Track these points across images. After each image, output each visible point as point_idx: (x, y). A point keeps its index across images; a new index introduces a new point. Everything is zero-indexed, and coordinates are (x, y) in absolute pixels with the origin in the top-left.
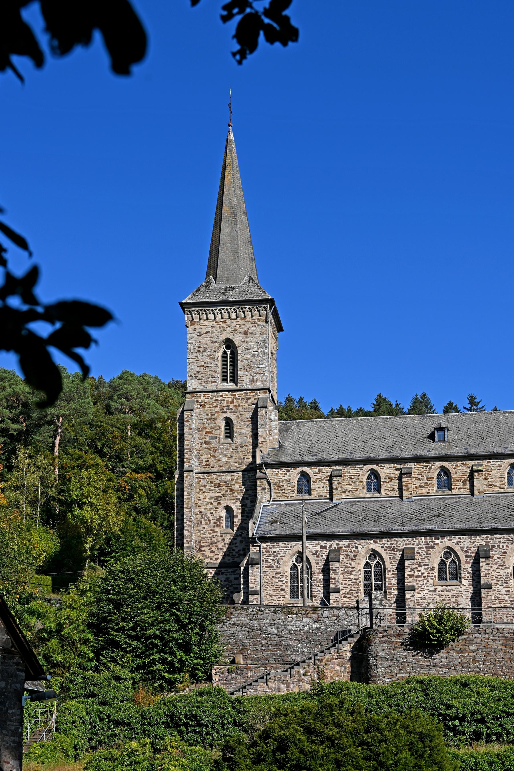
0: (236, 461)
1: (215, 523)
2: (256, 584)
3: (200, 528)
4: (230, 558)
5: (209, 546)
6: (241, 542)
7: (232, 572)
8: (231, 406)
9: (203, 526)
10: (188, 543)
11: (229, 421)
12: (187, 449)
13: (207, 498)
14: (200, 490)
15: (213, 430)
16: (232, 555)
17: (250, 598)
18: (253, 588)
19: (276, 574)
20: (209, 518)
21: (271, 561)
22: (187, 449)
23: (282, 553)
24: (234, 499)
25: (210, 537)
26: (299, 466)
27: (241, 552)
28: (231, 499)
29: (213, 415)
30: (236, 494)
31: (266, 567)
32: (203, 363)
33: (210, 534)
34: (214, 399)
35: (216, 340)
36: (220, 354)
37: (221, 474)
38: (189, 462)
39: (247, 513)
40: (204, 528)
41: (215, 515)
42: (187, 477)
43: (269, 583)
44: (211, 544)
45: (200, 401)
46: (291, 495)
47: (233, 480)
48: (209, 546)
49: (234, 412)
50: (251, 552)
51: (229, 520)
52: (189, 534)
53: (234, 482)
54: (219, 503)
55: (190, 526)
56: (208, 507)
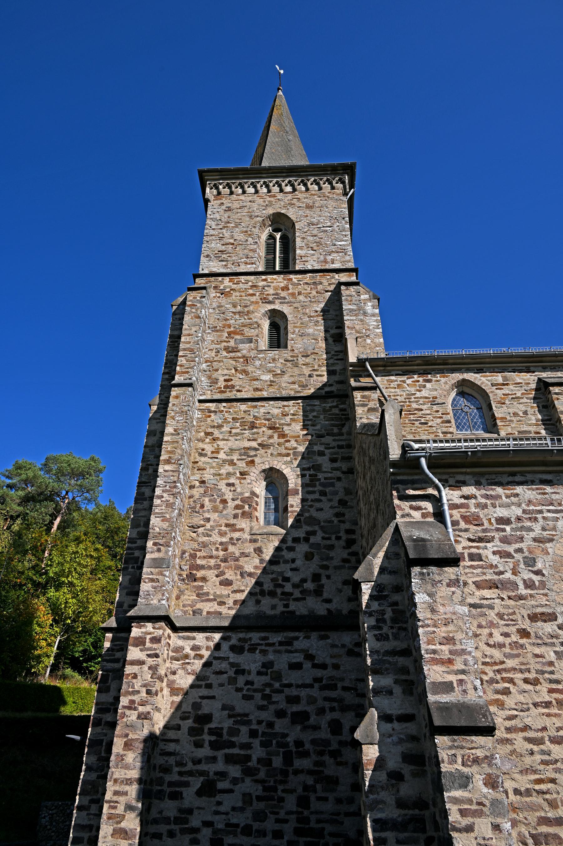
0: (292, 379)
1: (237, 507)
2: (459, 665)
3: (198, 520)
4: (275, 601)
5: (217, 567)
6: (308, 557)
7: (281, 643)
8: (283, 294)
9: (207, 515)
10: (159, 550)
11: (277, 320)
12: (184, 350)
13: (222, 452)
14: (207, 434)
15: (246, 330)
16: (283, 593)
17: (443, 755)
18: (448, 687)
19: (533, 618)
20: (223, 494)
21: (495, 559)
22: (184, 350)
23: (537, 527)
24: (288, 455)
25: (221, 544)
26: (453, 371)
27: (309, 585)
28: (280, 455)
29: (246, 306)
30: (293, 443)
31: (479, 585)
32: (232, 241)
33: (222, 534)
34: (250, 284)
35: (256, 214)
36: (264, 236)
37: (259, 403)
38: (188, 372)
39: (322, 485)
40: (208, 520)
41: (239, 490)
42: (177, 397)
43: (510, 663)
44: (225, 560)
45: (222, 288)
46: (445, 430)
47: (287, 415)
48: (217, 567)
49: (288, 303)
50: (399, 520)
51: (273, 506)
52: (165, 525)
53: (288, 419)
54: (252, 463)
55: (170, 505)
56: (223, 471)
